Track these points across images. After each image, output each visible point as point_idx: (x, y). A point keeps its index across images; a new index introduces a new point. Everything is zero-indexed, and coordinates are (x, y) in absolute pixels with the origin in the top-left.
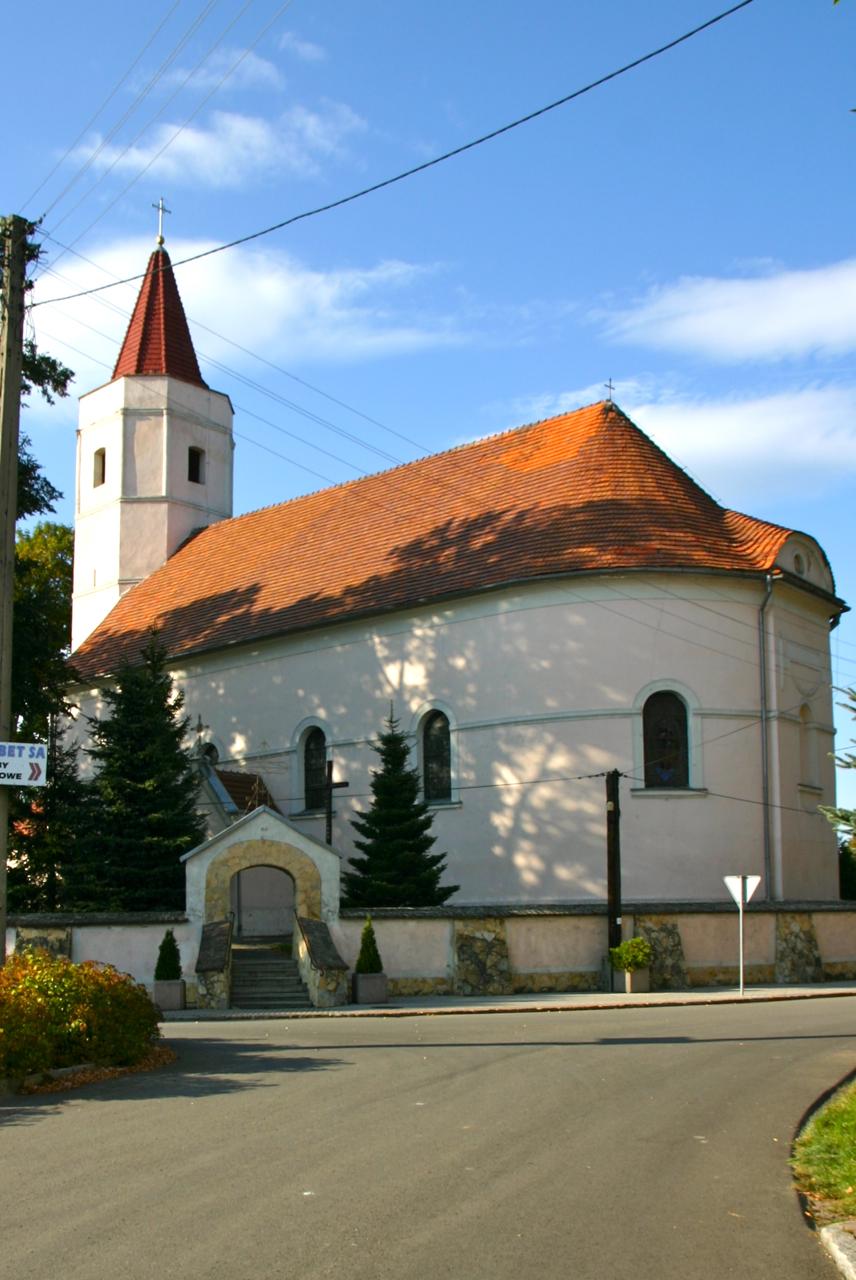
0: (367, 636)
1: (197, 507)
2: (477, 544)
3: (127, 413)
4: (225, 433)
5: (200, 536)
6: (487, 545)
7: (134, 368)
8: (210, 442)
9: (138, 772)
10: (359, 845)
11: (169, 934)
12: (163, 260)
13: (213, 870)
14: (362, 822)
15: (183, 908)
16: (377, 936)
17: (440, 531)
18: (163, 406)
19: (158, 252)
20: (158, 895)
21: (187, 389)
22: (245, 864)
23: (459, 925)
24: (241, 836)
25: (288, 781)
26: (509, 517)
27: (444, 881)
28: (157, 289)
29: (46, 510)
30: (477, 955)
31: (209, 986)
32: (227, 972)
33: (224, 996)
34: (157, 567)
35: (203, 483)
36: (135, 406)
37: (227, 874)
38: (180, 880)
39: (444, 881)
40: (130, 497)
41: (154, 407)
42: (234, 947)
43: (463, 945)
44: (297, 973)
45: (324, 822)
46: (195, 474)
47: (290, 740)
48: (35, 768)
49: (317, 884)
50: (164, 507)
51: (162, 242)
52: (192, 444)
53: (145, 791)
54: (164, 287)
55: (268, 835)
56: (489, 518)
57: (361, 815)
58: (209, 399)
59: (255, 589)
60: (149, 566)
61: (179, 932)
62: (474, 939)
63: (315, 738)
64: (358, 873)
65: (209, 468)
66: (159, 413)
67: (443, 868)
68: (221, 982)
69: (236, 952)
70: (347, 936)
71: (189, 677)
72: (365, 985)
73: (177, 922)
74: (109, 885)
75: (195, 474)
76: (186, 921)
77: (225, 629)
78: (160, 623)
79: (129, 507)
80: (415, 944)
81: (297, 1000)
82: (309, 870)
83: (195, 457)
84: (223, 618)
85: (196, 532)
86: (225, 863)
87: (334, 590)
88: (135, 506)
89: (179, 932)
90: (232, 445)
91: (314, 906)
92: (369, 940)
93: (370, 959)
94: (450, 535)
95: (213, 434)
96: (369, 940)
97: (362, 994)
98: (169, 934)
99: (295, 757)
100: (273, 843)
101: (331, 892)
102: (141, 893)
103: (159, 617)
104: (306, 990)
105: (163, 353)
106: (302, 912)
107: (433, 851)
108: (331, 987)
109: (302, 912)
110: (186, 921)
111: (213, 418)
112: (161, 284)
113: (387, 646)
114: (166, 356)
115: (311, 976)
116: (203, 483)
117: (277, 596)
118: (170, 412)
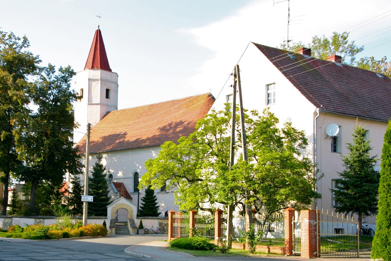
0: (151, 150)
1: (108, 105)
2: (178, 130)
3: (89, 80)
4: (116, 84)
5: (109, 114)
6: (180, 131)
7: (91, 67)
8: (111, 87)
9: (98, 188)
10: (142, 204)
11: (105, 221)
12: (99, 36)
13: (112, 209)
14: (143, 199)
15: (107, 216)
16: (143, 222)
17: (170, 125)
18: (99, 78)
19: (98, 30)
20: (104, 214)
21: (106, 72)
22: (119, 208)
23: (160, 220)
24: (118, 203)
25: (130, 187)
26: (186, 123)
27: (159, 212)
28: (98, 42)
29: (77, 128)
30: (163, 226)
31: (112, 230)
32: (115, 228)
33: (114, 232)
34: (97, 123)
35: (110, 99)
36: (91, 78)
37: (115, 210)
38: (106, 210)
39: (159, 212)
40: (90, 103)
41: (97, 78)
42: (116, 224)
43: (160, 224)
44: (128, 229)
45: (137, 196)
46: (107, 96)
47: (131, 175)
48: (91, 199)
49: (132, 212)
50: (99, 106)
51: (99, 27)
52: (107, 88)
53: (99, 193)
54: (99, 41)
55: (123, 202)
56: (181, 123)
57: (143, 197)
58: (112, 75)
59: (125, 134)
60: (95, 122)
61: (106, 220)
62: (162, 223)
63: (136, 175)
64: (142, 209)
65: (111, 94)
66: (98, 80)
67: (158, 209)
68: (114, 230)
69: (117, 225)
70: (137, 222)
71: (108, 155)
72: (141, 231)
73: (105, 218)
74: (92, 211)
75: (107, 96)
76: (107, 218)
77: (117, 145)
78: (101, 140)
79: (90, 106)
80: (150, 223)
81: (128, 234)
82: (131, 209)
83: (108, 91)
84: (117, 141)
85: (108, 113)
86: (115, 208)
87: (145, 138)
88: (91, 105)
89: (106, 220)
90: (118, 86)
91: (132, 216)
92: (141, 222)
93: (141, 226)
94: (172, 126)
95: (112, 84)
96: (141, 222)
97: (139, 232)
98: (105, 221)
99: (131, 179)
100: (124, 204)
101: (135, 213)
102: (98, 213)
103: (100, 138)
104: (129, 232)
105: (99, 61)
106: (129, 217)
107: (157, 205)
108: (134, 231)
109: (129, 217)
110: (107, 218)
111: (112, 80)
112: (99, 40)
113: (156, 154)
114: (100, 62)
115: (130, 229)
116: (110, 99)
117: (131, 137)
118: (101, 79)
